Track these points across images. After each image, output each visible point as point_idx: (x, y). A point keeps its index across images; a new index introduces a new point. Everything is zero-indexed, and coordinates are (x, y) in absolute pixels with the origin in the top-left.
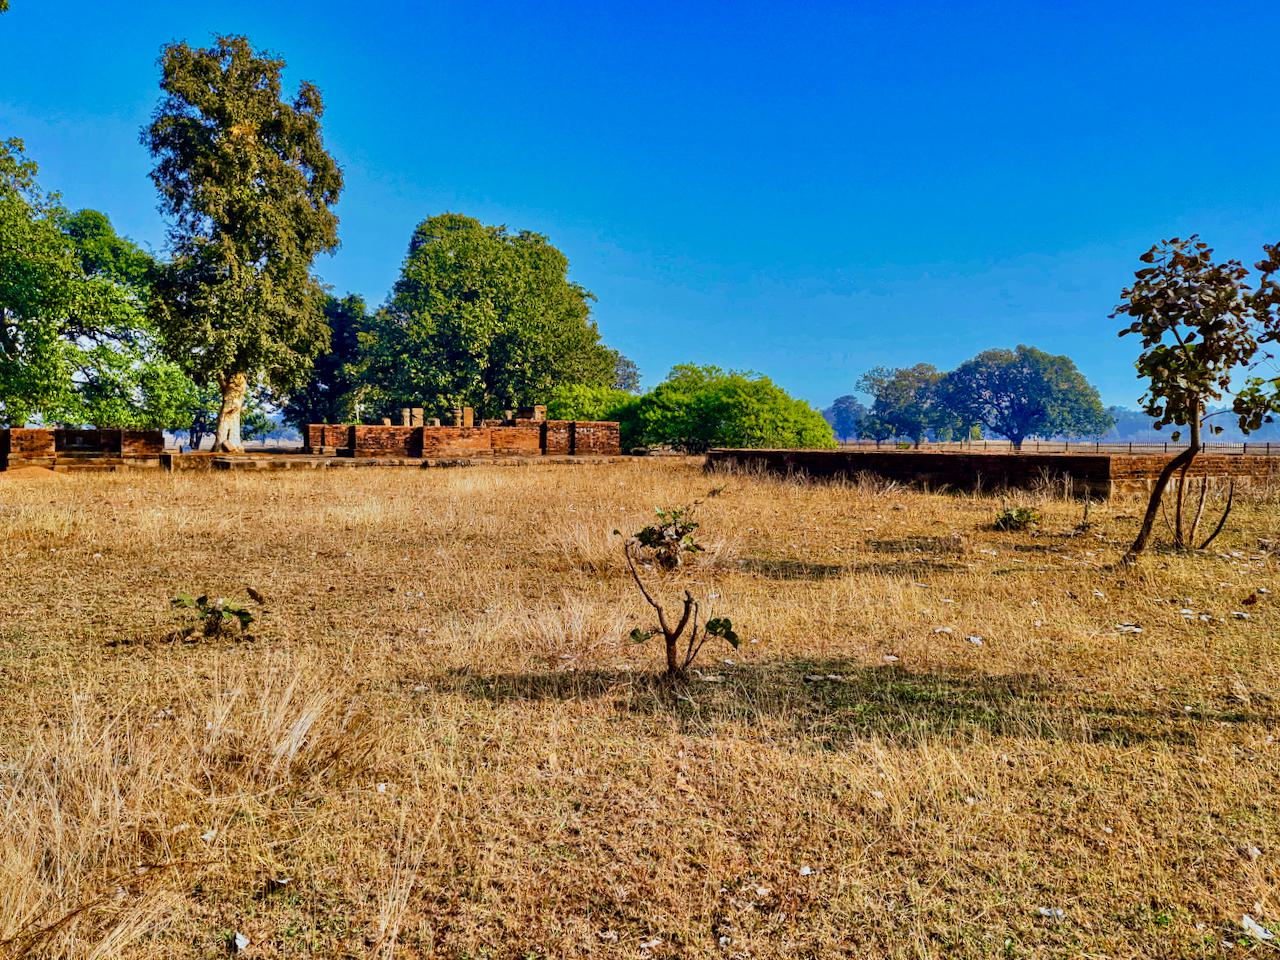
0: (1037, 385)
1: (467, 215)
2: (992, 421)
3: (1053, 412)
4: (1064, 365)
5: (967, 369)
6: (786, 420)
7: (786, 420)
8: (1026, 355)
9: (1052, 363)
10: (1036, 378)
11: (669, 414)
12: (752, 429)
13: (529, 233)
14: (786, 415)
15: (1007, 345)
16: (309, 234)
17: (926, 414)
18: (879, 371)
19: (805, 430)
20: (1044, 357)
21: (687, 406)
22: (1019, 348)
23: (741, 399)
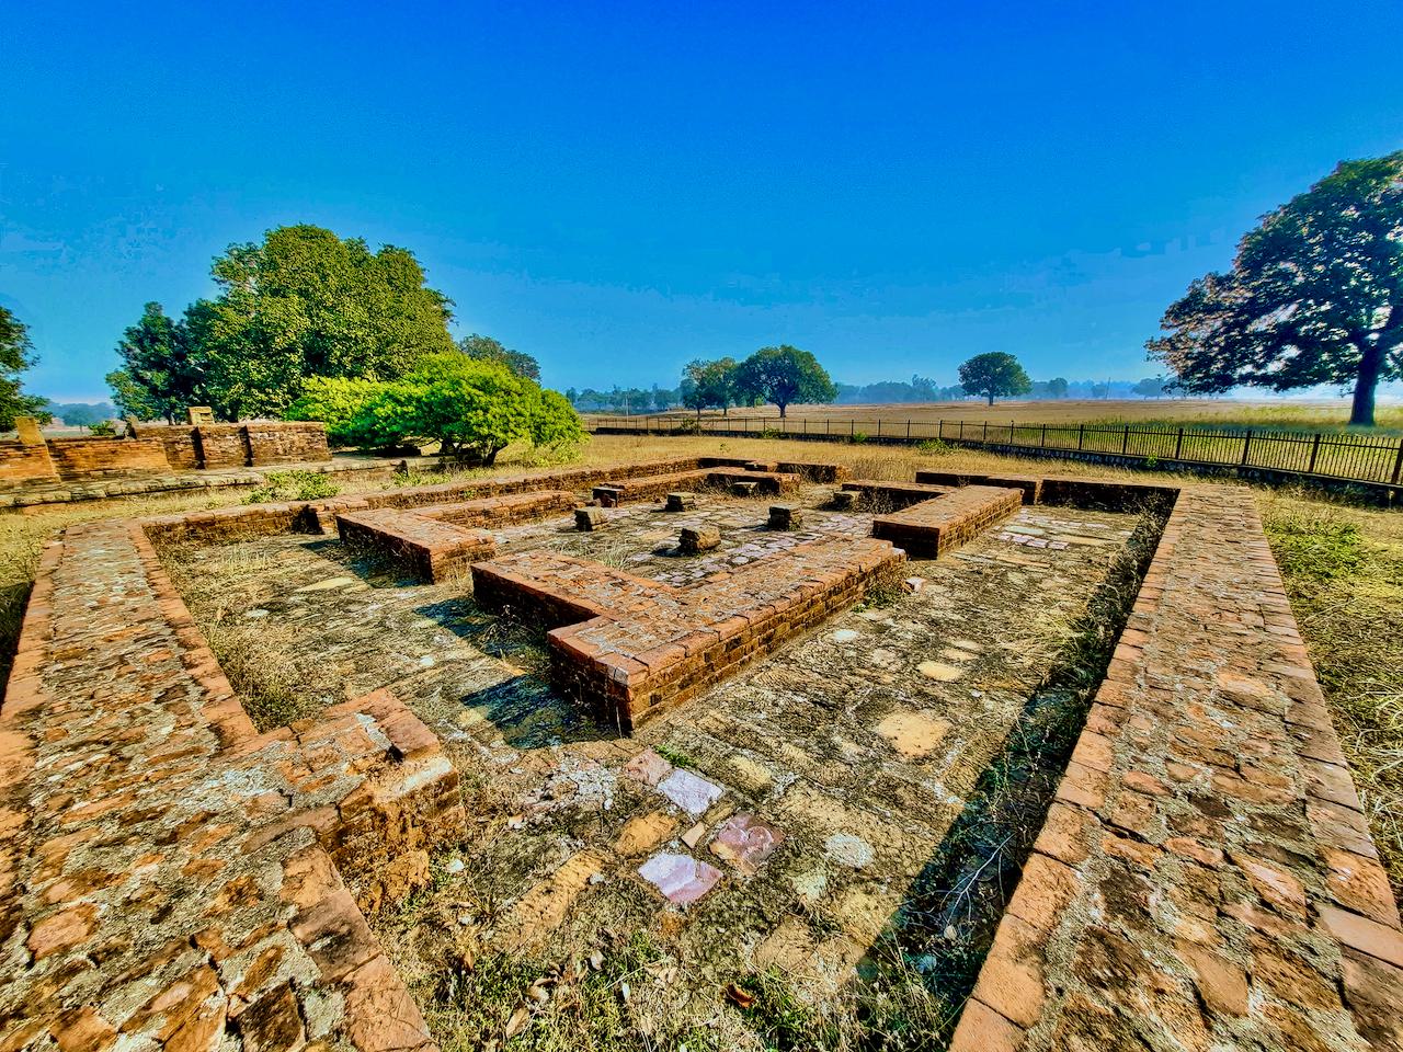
0: (794, 371)
1: (320, 226)
2: (767, 394)
3: (803, 388)
4: (809, 357)
5: (752, 361)
6: (520, 414)
7: (520, 414)
8: (788, 352)
9: (802, 356)
10: (793, 367)
11: (399, 409)
12: (480, 426)
13: (392, 247)
14: (519, 408)
15: (774, 343)
16: (417, 279)
17: (730, 389)
18: (697, 362)
19: (545, 424)
20: (798, 352)
21: (419, 400)
22: (389, 249)
23: (464, 392)
